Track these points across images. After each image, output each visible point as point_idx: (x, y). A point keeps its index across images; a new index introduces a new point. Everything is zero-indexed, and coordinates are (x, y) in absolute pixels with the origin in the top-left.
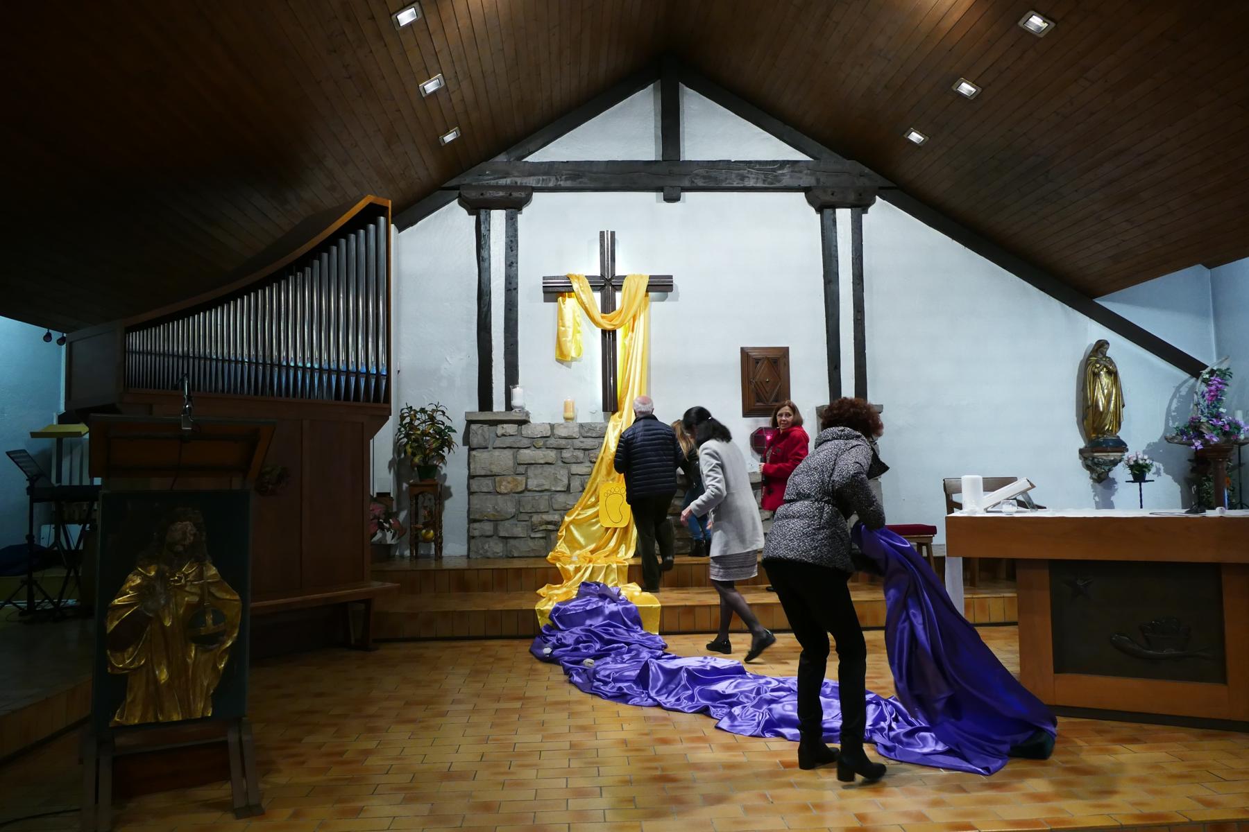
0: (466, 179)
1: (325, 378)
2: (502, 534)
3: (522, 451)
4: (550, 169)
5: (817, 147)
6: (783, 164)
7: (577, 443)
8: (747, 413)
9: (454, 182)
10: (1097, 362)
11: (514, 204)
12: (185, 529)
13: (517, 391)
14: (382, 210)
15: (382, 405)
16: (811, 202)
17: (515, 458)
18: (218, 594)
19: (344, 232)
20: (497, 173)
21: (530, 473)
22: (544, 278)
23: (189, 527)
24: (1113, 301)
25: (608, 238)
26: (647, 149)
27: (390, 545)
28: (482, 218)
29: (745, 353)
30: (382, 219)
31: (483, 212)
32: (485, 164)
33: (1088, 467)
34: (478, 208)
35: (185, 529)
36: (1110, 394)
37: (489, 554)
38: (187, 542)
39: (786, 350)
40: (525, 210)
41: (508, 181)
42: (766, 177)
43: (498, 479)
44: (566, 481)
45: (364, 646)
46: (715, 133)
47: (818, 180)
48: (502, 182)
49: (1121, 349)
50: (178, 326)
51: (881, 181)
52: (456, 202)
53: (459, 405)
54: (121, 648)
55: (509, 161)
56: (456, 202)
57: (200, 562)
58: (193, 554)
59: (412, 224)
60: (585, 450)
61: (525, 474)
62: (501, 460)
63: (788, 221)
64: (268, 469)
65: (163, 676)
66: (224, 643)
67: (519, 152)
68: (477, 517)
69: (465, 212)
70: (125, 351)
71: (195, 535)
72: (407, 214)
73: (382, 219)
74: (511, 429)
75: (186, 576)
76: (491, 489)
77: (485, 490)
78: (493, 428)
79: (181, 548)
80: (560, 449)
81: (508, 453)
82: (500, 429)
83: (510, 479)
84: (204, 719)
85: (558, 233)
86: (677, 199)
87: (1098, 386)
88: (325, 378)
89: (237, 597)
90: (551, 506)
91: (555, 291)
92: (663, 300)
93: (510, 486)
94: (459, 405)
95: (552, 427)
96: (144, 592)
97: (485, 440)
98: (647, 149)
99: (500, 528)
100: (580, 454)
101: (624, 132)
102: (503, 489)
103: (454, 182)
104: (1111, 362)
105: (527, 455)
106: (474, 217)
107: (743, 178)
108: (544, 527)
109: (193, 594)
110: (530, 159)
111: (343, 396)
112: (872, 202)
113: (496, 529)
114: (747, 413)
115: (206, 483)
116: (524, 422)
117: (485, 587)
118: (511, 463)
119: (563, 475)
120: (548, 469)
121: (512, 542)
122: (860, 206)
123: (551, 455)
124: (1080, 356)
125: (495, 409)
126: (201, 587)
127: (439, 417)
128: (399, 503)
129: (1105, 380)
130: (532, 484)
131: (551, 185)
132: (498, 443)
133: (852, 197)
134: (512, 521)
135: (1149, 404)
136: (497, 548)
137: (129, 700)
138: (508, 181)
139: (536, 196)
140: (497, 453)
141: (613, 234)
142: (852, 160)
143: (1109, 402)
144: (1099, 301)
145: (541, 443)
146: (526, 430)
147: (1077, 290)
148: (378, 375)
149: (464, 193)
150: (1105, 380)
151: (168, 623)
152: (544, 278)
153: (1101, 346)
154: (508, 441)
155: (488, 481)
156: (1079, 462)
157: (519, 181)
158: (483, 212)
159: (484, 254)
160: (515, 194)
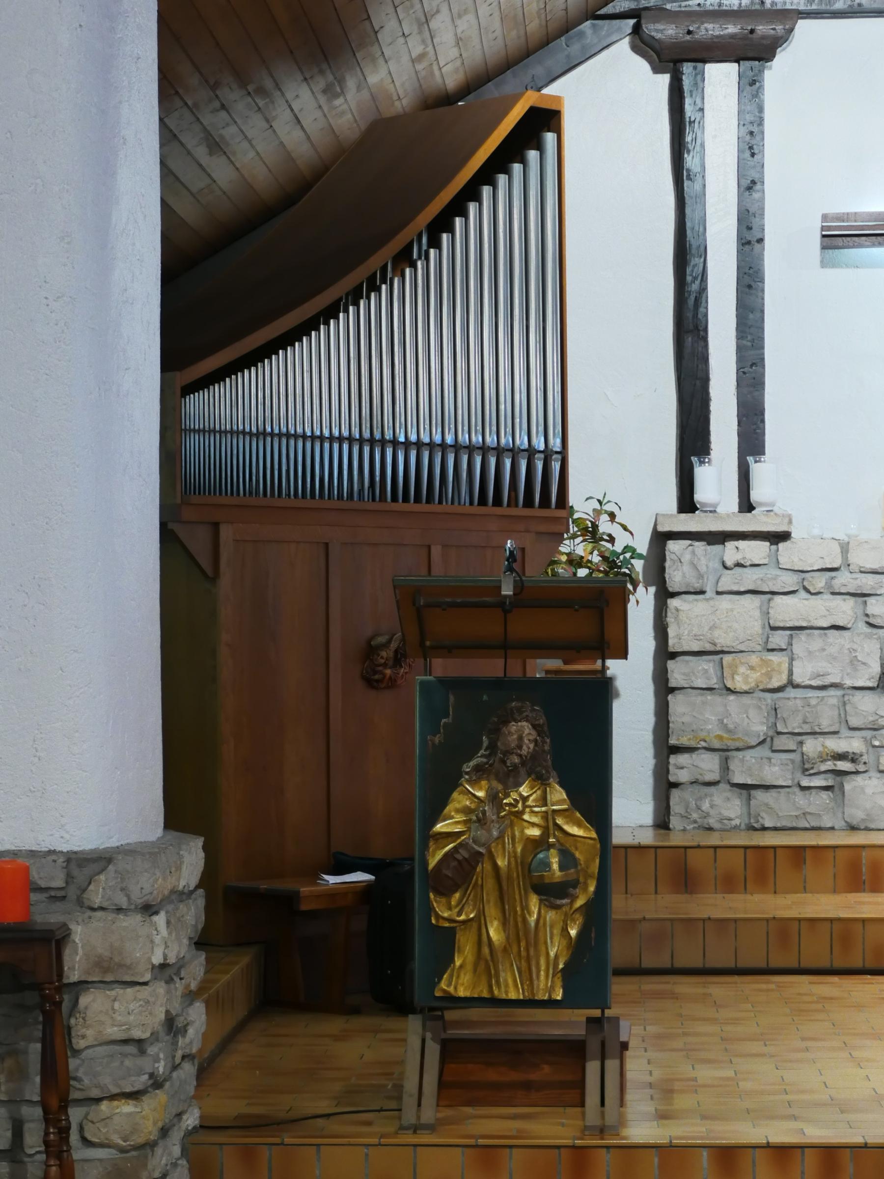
2: (739, 779)
3: (778, 599)
11: (753, 50)
12: (522, 733)
13: (759, 470)
15: (553, 512)
18: (566, 828)
19: (487, 174)
22: (825, 217)
23: (526, 728)
31: (687, 68)
35: (522, 733)
37: (712, 822)
38: (524, 751)
43: (727, 659)
50: (249, 376)
54: (445, 892)
56: (625, 44)
57: (541, 780)
64: (381, 640)
65: (495, 933)
66: (574, 898)
68: (684, 741)
71: (536, 741)
74: (756, 550)
75: (525, 799)
76: (713, 682)
77: (700, 683)
78: (717, 548)
79: (516, 760)
81: (751, 603)
82: (731, 552)
83: (754, 659)
84: (551, 1003)
89: (594, 835)
93: (754, 676)
96: (476, 818)
97: (701, 576)
99: (734, 765)
102: (739, 683)
105: (788, 610)
106: (665, 79)
108: (829, 765)
109: (533, 825)
113: (725, 768)
115: (543, 666)
116: (779, 537)
117: (729, 884)
118: (756, 627)
121: (759, 794)
123: (844, 610)
126: (545, 816)
127: (605, 526)
132: (728, 581)
134: (764, 751)
136: (727, 808)
137: (458, 963)
139: (803, 26)
140: (725, 602)
145: (819, 582)
149: (652, 29)
151: (501, 863)
152: (825, 217)
154: (749, 579)
155: (707, 665)
158: (687, 68)
159: (691, 161)
160: (763, 29)
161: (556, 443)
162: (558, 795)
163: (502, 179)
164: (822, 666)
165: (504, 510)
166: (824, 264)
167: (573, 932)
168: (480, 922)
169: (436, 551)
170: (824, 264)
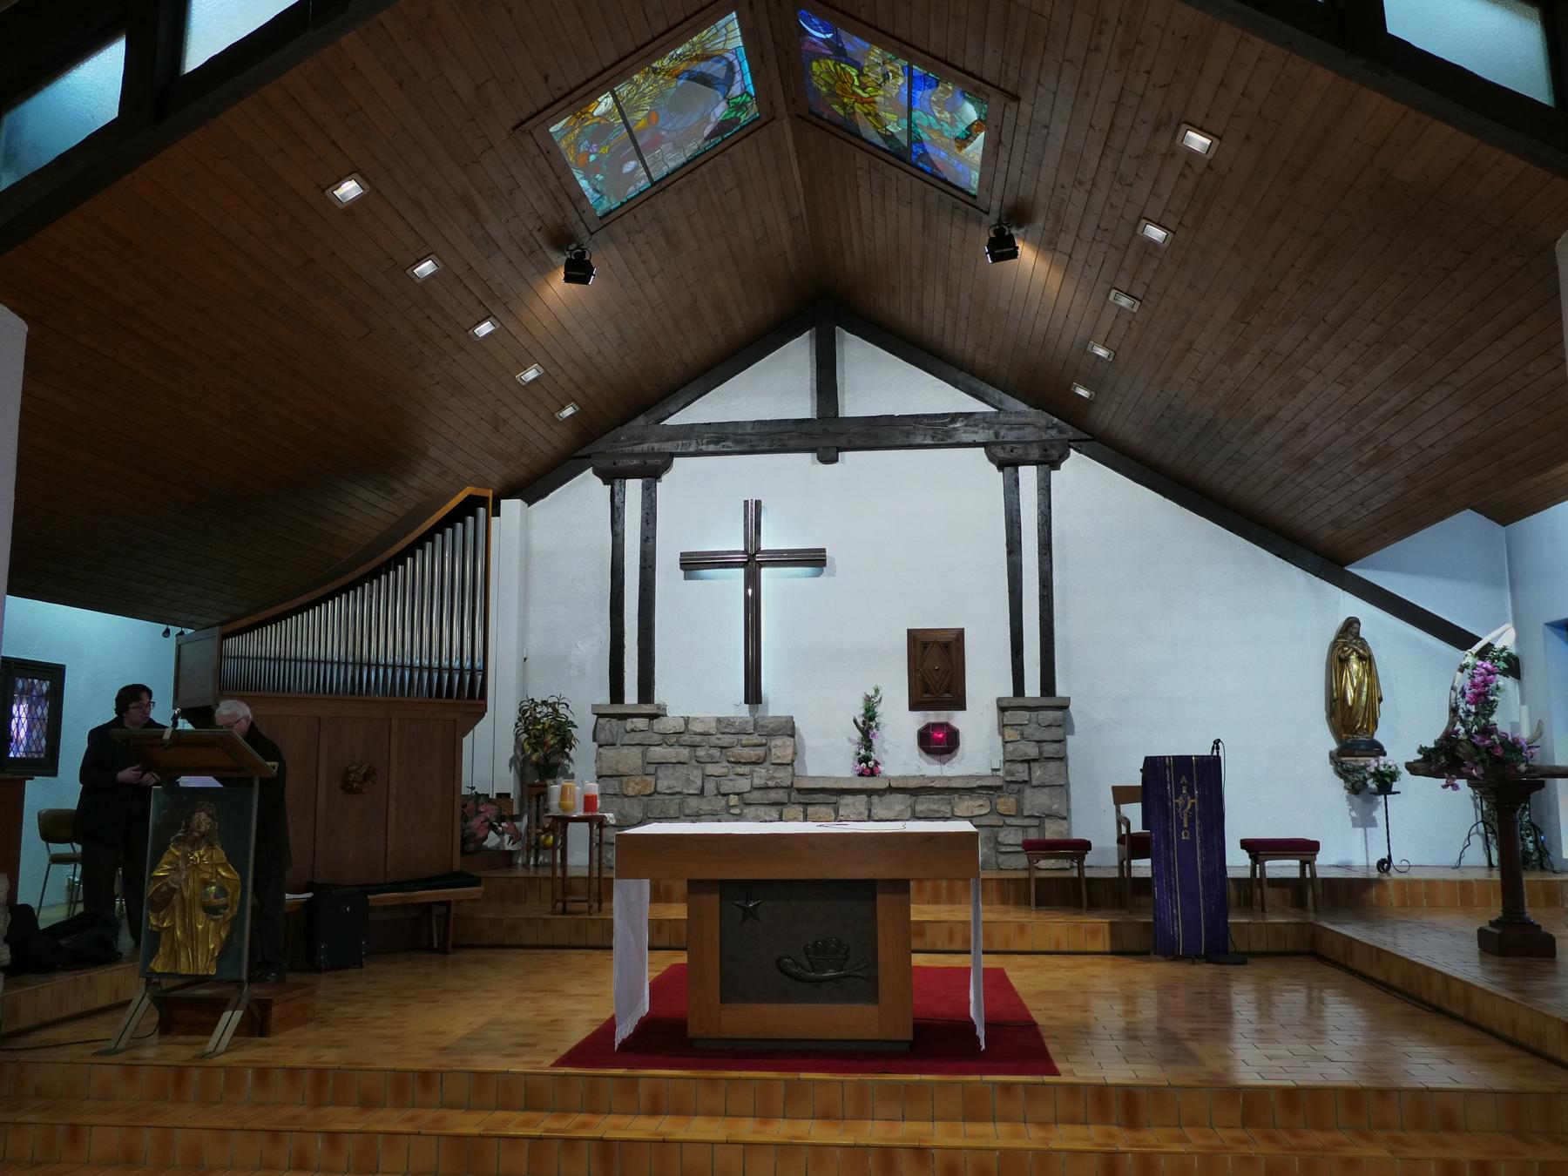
0: (600, 446)
1: (416, 675)
4: (691, 431)
5: (997, 394)
6: (955, 417)
7: (713, 740)
8: (915, 705)
9: (586, 451)
10: (1345, 645)
11: (652, 472)
14: (482, 501)
15: (477, 702)
16: (992, 458)
17: (644, 755)
19: (440, 527)
20: (635, 439)
21: (660, 774)
23: (203, 816)
24: (1375, 568)
25: (752, 507)
26: (802, 407)
27: (511, 853)
28: (617, 488)
29: (912, 634)
30: (482, 510)
31: (617, 482)
32: (619, 429)
33: (1341, 775)
34: (612, 476)
36: (1360, 684)
38: (203, 829)
39: (961, 632)
40: (665, 477)
41: (646, 447)
42: (931, 432)
44: (699, 783)
45: (443, 950)
46: (879, 383)
47: (997, 435)
48: (637, 449)
49: (1376, 624)
50: (270, 630)
51: (1071, 432)
52: (590, 470)
53: (584, 696)
55: (647, 425)
56: (590, 470)
57: (211, 845)
58: (207, 839)
59: (542, 497)
60: (722, 748)
61: (654, 774)
62: (630, 758)
63: (968, 477)
67: (657, 415)
69: (600, 481)
70: (221, 656)
72: (533, 487)
73: (482, 510)
74: (641, 723)
80: (693, 746)
81: (637, 751)
82: (630, 724)
85: (700, 501)
86: (835, 460)
87: (1346, 674)
88: (416, 675)
90: (681, 810)
91: (692, 564)
92: (817, 575)
94: (584, 696)
95: (687, 721)
98: (802, 407)
100: (716, 753)
101: (776, 387)
102: (630, 791)
103: (586, 451)
104: (1364, 644)
105: (657, 753)
107: (908, 435)
110: (670, 421)
111: (441, 693)
112: (1064, 456)
114: (915, 705)
119: (696, 776)
120: (681, 769)
122: (1050, 462)
123: (685, 753)
124: (1331, 637)
125: (627, 701)
127: (562, 710)
128: (521, 806)
129: (1355, 666)
130: (663, 785)
131: (692, 449)
132: (627, 739)
133: (1035, 453)
135: (1416, 698)
138: (646, 447)
140: (625, 750)
141: (758, 503)
142: (1042, 407)
143: (1360, 695)
144: (1348, 569)
146: (659, 725)
147: (1328, 559)
148: (473, 670)
150: (1355, 666)
151: (187, 894)
153: (1351, 625)
154: (638, 738)
156: (1331, 768)
157: (656, 446)
158: (617, 482)
160: (651, 462)
161: (478, 664)
162: (219, 854)
163: (449, 531)
164: (672, 782)
165: (444, 700)
166: (686, 578)
167: (223, 935)
168: (172, 929)
169: (395, 722)
170: (686, 578)
